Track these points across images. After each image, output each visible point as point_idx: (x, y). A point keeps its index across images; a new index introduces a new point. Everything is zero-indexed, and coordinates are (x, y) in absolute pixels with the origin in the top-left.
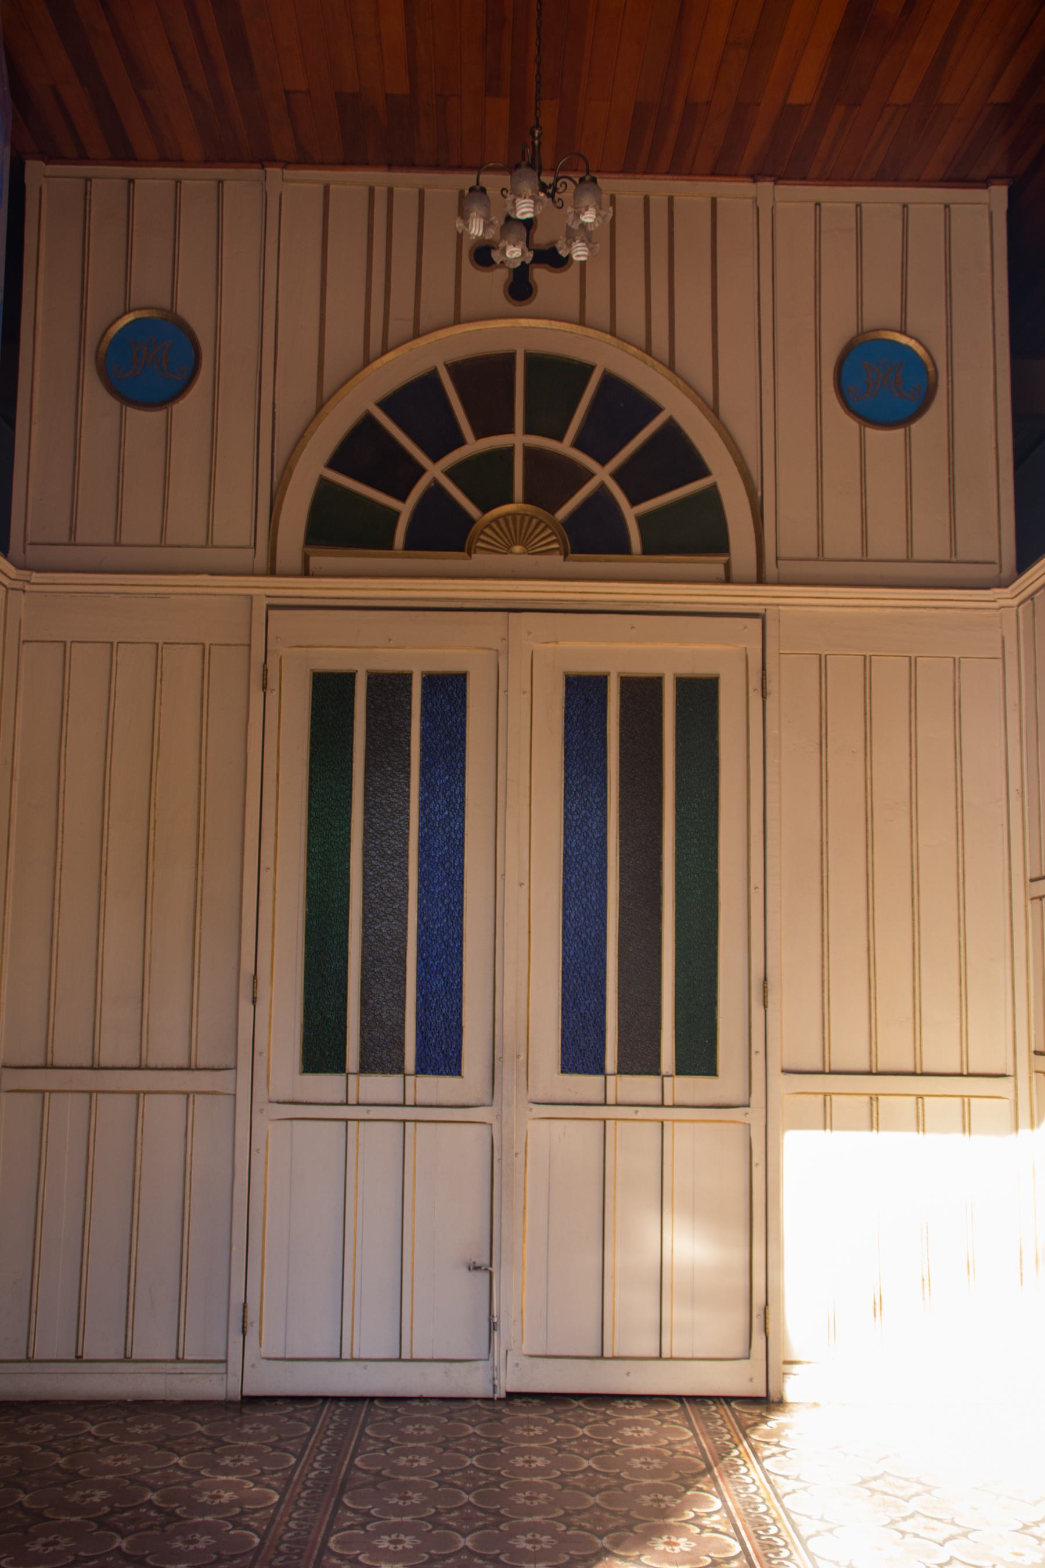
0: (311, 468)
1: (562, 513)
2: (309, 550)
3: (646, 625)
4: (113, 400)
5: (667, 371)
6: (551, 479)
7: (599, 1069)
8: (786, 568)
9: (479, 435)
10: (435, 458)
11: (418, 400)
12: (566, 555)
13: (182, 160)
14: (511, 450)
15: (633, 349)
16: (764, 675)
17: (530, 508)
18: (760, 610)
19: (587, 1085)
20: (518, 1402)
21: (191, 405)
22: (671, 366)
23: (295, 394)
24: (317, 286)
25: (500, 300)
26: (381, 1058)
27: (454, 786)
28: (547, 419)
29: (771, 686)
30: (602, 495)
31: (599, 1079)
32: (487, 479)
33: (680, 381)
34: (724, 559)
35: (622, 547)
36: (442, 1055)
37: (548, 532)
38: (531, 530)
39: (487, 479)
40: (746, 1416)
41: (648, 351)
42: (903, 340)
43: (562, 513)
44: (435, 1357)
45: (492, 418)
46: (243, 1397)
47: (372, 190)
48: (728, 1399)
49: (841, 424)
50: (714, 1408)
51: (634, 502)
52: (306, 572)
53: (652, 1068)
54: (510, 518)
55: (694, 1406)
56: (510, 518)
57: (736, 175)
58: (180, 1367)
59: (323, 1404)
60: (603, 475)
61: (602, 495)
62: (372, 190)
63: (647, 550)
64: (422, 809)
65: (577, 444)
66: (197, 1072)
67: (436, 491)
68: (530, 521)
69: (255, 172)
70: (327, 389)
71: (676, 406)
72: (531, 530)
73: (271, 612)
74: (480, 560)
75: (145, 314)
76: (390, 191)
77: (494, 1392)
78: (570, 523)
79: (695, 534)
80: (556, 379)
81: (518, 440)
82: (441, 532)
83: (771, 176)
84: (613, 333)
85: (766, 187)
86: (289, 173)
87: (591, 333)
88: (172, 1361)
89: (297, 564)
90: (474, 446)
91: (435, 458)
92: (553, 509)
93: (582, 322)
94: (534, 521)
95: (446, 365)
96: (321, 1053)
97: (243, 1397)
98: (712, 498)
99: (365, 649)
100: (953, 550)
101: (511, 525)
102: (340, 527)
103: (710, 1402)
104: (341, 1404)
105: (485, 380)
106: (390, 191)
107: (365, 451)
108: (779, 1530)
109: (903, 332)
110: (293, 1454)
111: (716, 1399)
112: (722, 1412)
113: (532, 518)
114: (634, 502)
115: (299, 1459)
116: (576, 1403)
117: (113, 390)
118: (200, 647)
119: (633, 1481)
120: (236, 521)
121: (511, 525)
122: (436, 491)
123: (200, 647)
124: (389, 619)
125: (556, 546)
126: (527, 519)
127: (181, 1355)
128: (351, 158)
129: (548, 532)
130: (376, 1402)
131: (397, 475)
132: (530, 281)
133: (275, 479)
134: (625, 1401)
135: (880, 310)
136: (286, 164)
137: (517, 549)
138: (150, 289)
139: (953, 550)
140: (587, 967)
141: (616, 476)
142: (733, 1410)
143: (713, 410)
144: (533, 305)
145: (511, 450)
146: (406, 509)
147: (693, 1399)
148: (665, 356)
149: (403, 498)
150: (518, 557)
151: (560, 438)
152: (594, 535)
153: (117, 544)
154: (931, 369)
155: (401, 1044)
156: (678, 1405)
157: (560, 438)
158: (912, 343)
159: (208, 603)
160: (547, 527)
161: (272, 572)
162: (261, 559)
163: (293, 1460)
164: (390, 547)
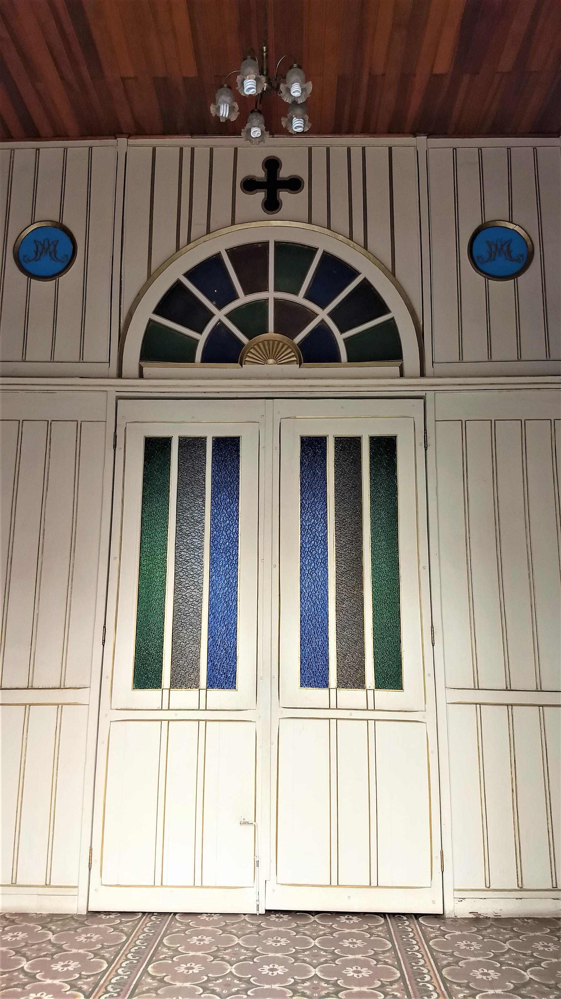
0: (145, 314)
1: (298, 339)
2: (143, 364)
3: (347, 404)
4: (24, 275)
5: (363, 250)
6: (290, 318)
7: (325, 684)
8: (438, 368)
9: (200, 332)
10: (220, 307)
11: (208, 273)
12: (300, 364)
13: (68, 136)
14: (267, 300)
15: (341, 237)
16: (425, 433)
17: (278, 336)
18: (422, 394)
19: (317, 696)
20: (273, 917)
21: (71, 278)
22: (366, 247)
23: (135, 277)
24: (149, 207)
25: (260, 211)
26: (183, 679)
27: (232, 506)
28: (289, 280)
29: (430, 441)
30: (322, 328)
31: (326, 691)
32: (251, 319)
33: (371, 256)
34: (399, 363)
35: (336, 358)
36: (223, 675)
37: (289, 350)
38: (278, 350)
39: (251, 319)
40: (429, 929)
41: (351, 238)
42: (511, 226)
43: (298, 339)
44: (217, 885)
45: (254, 284)
46: (88, 912)
47: (181, 150)
48: (417, 916)
49: (473, 279)
50: (407, 923)
51: (342, 331)
52: (141, 376)
53: (360, 684)
54: (266, 342)
55: (393, 920)
56: (266, 342)
57: (403, 133)
58: (47, 890)
59: (142, 917)
60: (323, 315)
61: (322, 328)
62: (181, 150)
63: (351, 359)
64: (212, 520)
65: (307, 297)
66: (64, 690)
67: (220, 326)
68: (278, 344)
69: (112, 141)
70: (154, 267)
71: (368, 271)
72: (278, 350)
73: (119, 401)
74: (247, 368)
75: (43, 224)
76: (193, 150)
77: (258, 910)
78: (303, 344)
79: (382, 347)
80: (294, 256)
81: (271, 295)
82: (223, 350)
83: (425, 133)
84: (329, 227)
85: (422, 139)
86: (131, 141)
87: (316, 228)
88: (42, 886)
89: (136, 372)
90: (243, 299)
91: (220, 307)
92: (293, 337)
93: (310, 222)
94: (281, 344)
95: (226, 250)
96: (146, 675)
97: (88, 912)
98: (391, 325)
99: (176, 423)
100: (548, 353)
101: (267, 347)
102: (160, 348)
103: (405, 918)
104: (153, 918)
105: (249, 257)
106: (193, 150)
107: (175, 303)
108: (425, 962)
109: (512, 223)
110: (126, 934)
111: (408, 915)
112: (413, 927)
113: (279, 342)
114: (342, 331)
115: (128, 937)
116: (313, 918)
117: (23, 270)
118: (76, 423)
119: (346, 989)
120: (99, 346)
121: (267, 347)
122: (220, 326)
123: (76, 423)
124: (192, 404)
125: (295, 359)
126: (276, 343)
127: (48, 883)
128: (169, 130)
129: (289, 350)
130: (177, 917)
131: (196, 317)
132: (278, 199)
133: (122, 321)
134: (346, 917)
135: (496, 211)
136: (129, 136)
137: (271, 361)
138: (48, 211)
139: (548, 353)
140: (316, 617)
141: (331, 315)
142: (420, 925)
143: (392, 274)
144: (282, 212)
145: (267, 300)
146: (202, 338)
147: (392, 915)
148: (362, 241)
149: (200, 332)
150: (271, 366)
151: (296, 293)
152: (318, 350)
153: (24, 361)
154: (529, 243)
155: (197, 670)
156: (382, 921)
157: (296, 293)
158: (517, 228)
159: (93, 400)
160: (289, 347)
161: (120, 376)
162: (114, 369)
163: (125, 938)
164: (193, 361)
